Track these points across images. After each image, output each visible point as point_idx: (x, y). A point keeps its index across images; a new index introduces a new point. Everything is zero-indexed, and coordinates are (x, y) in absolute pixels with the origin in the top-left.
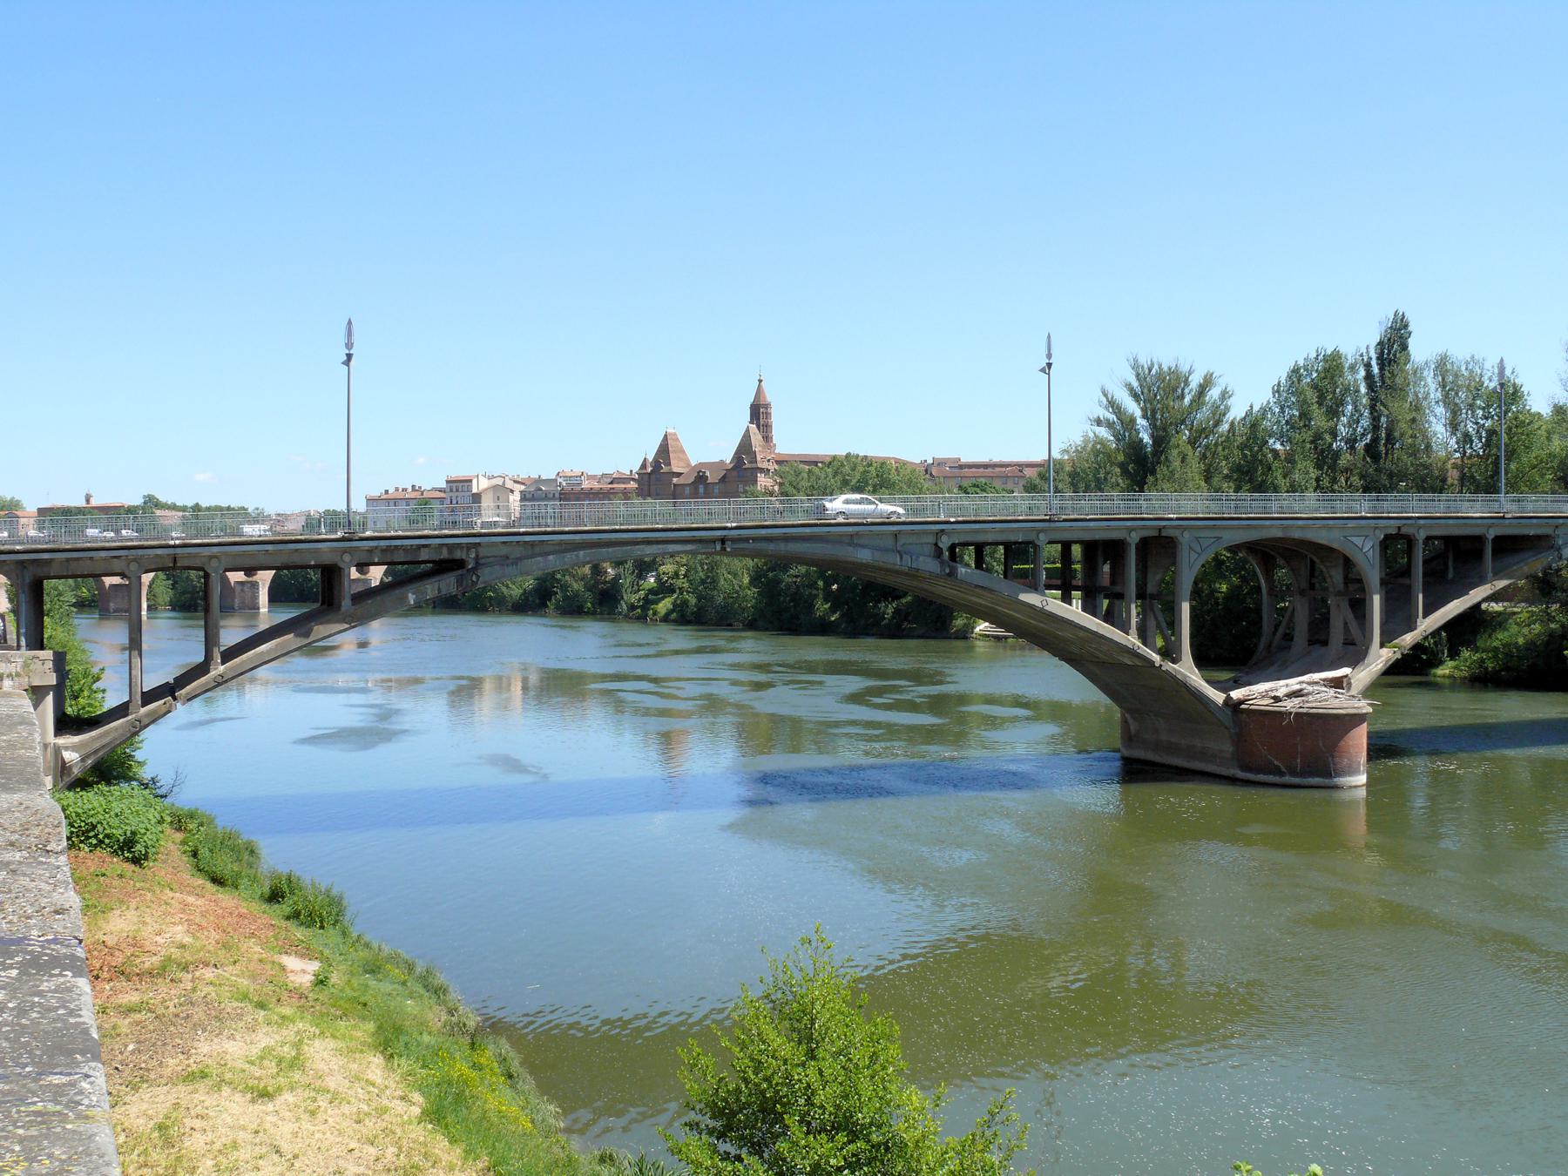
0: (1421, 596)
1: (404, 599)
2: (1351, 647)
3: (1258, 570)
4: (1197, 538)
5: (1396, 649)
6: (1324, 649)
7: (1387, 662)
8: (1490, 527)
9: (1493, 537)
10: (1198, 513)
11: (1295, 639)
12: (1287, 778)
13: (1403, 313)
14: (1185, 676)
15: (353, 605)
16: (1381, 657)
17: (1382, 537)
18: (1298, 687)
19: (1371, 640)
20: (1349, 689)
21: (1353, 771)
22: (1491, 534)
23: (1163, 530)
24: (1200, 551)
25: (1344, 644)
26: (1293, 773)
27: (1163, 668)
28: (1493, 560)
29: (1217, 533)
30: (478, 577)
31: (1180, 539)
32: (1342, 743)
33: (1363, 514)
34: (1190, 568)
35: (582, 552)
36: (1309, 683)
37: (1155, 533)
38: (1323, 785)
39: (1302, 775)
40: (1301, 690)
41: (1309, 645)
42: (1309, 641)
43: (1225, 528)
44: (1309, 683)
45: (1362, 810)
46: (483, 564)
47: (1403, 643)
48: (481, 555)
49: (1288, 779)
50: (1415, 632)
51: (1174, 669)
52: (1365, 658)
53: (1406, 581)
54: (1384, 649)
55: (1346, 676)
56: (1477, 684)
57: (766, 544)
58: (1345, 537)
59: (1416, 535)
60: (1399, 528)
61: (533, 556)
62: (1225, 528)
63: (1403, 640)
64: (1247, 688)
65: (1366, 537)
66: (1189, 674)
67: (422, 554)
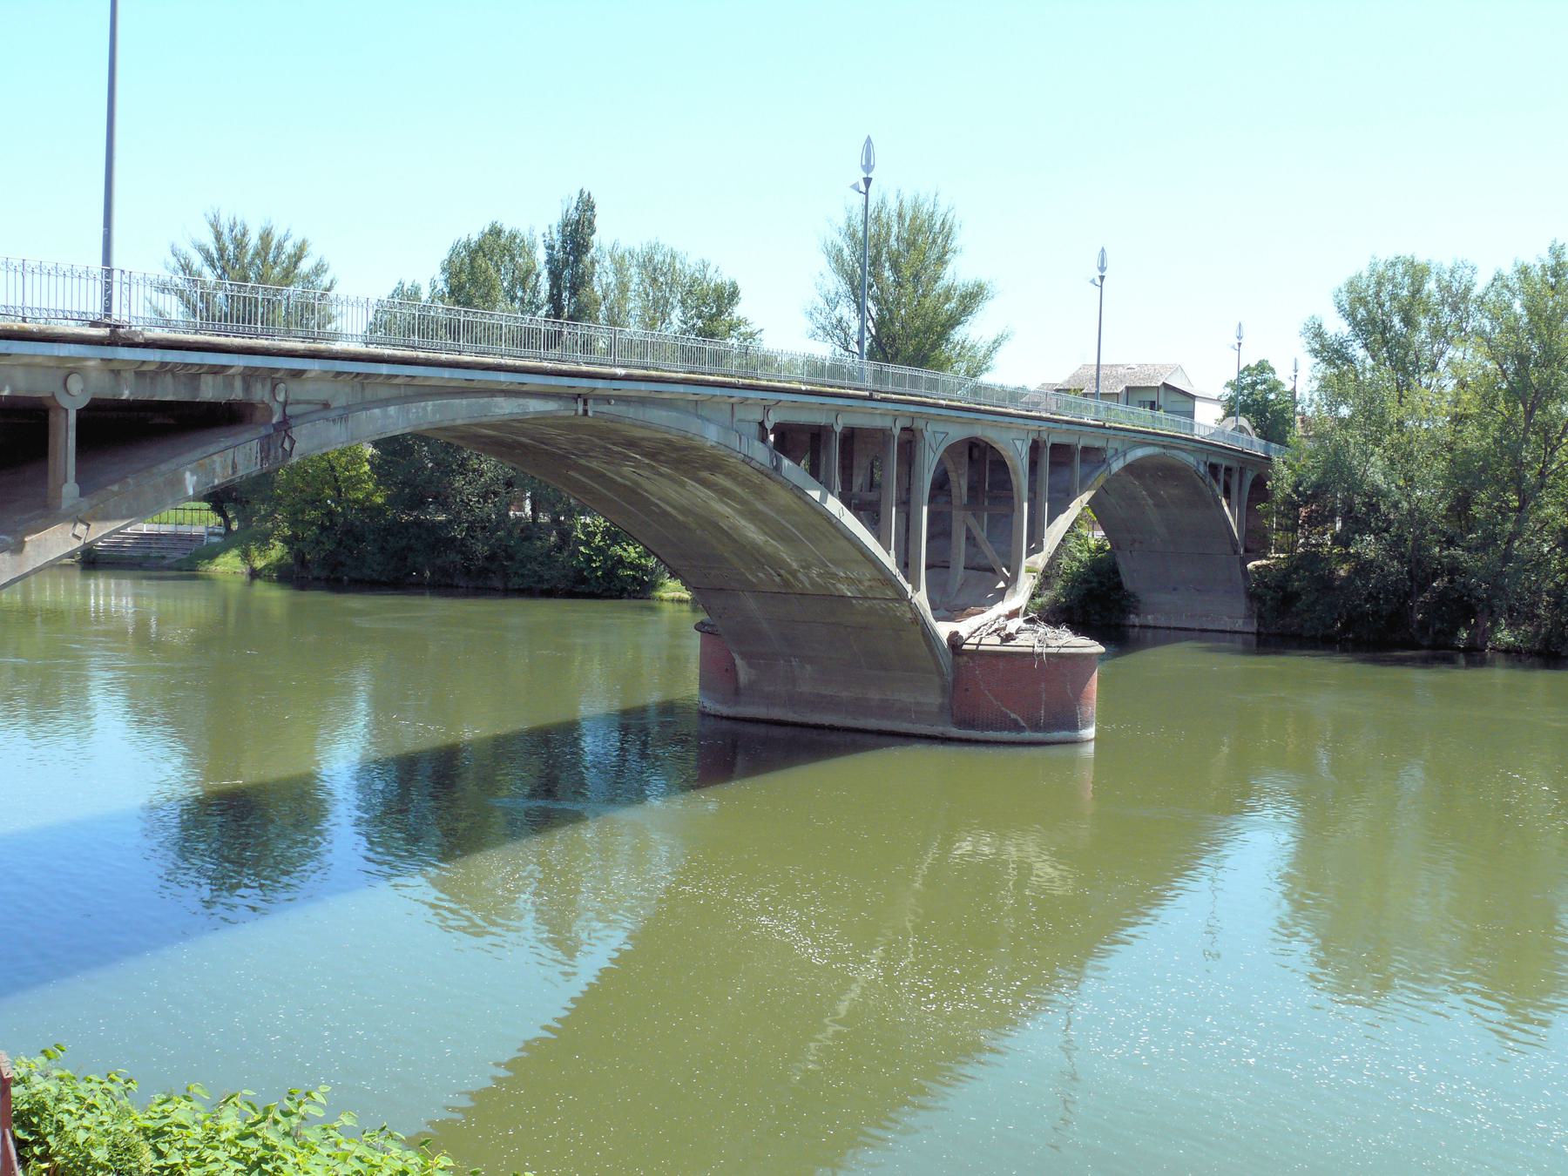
1: (178, 483)
9: (83, 402)
12: (1027, 734)
13: (589, 194)
15: (81, 495)
21: (1085, 726)
22: (74, 398)
26: (1036, 727)
28: (1051, 473)
30: (293, 442)
32: (1085, 690)
33: (1085, 420)
35: (430, 403)
38: (1069, 739)
39: (1048, 727)
45: (1091, 767)
46: (297, 417)
48: (291, 397)
49: (1028, 735)
57: (625, 408)
61: (367, 405)
67: (203, 387)
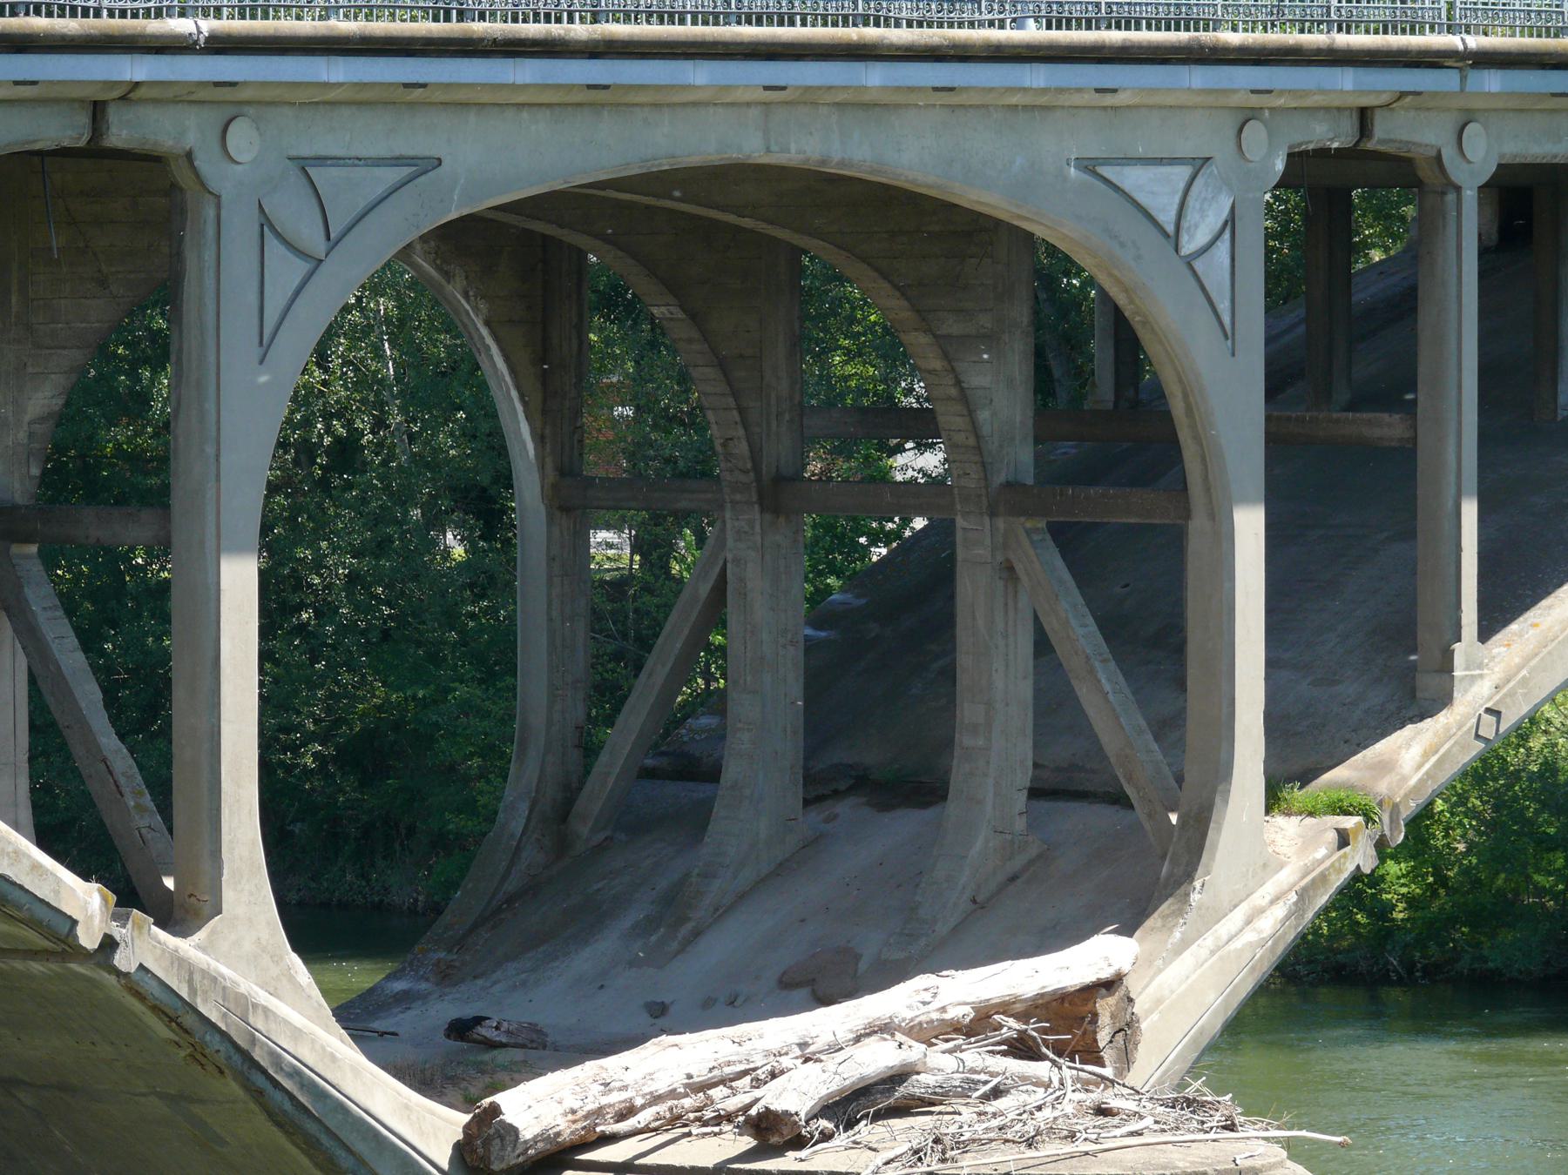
0: (1470, 512)
2: (1096, 818)
3: (496, 363)
4: (303, 165)
5: (1350, 822)
6: (905, 823)
7: (1304, 895)
8: (1248, 116)
9: (1487, 172)
10: (1217, 25)
11: (732, 770)
14: (244, 1005)
16: (1270, 866)
17: (1280, 165)
18: (877, 1058)
19: (1220, 771)
20: (1126, 1059)
23: (114, 115)
24: (318, 246)
25: (1035, 793)
27: (124, 960)
29: (415, 138)
31: (208, 164)
34: (265, 345)
36: (927, 1033)
37: (64, 131)
40: (899, 1077)
41: (807, 803)
42: (809, 779)
43: (460, 103)
44: (927, 1033)
47: (1383, 787)
50: (1443, 719)
51: (180, 962)
52: (1189, 876)
53: (1387, 427)
54: (1279, 820)
55: (1109, 985)
56: (1325, 994)
58: (1089, 166)
59: (1448, 154)
60: (1364, 116)
62: (460, 103)
63: (1385, 766)
64: (590, 1068)
65: (1200, 164)
66: (263, 997)
